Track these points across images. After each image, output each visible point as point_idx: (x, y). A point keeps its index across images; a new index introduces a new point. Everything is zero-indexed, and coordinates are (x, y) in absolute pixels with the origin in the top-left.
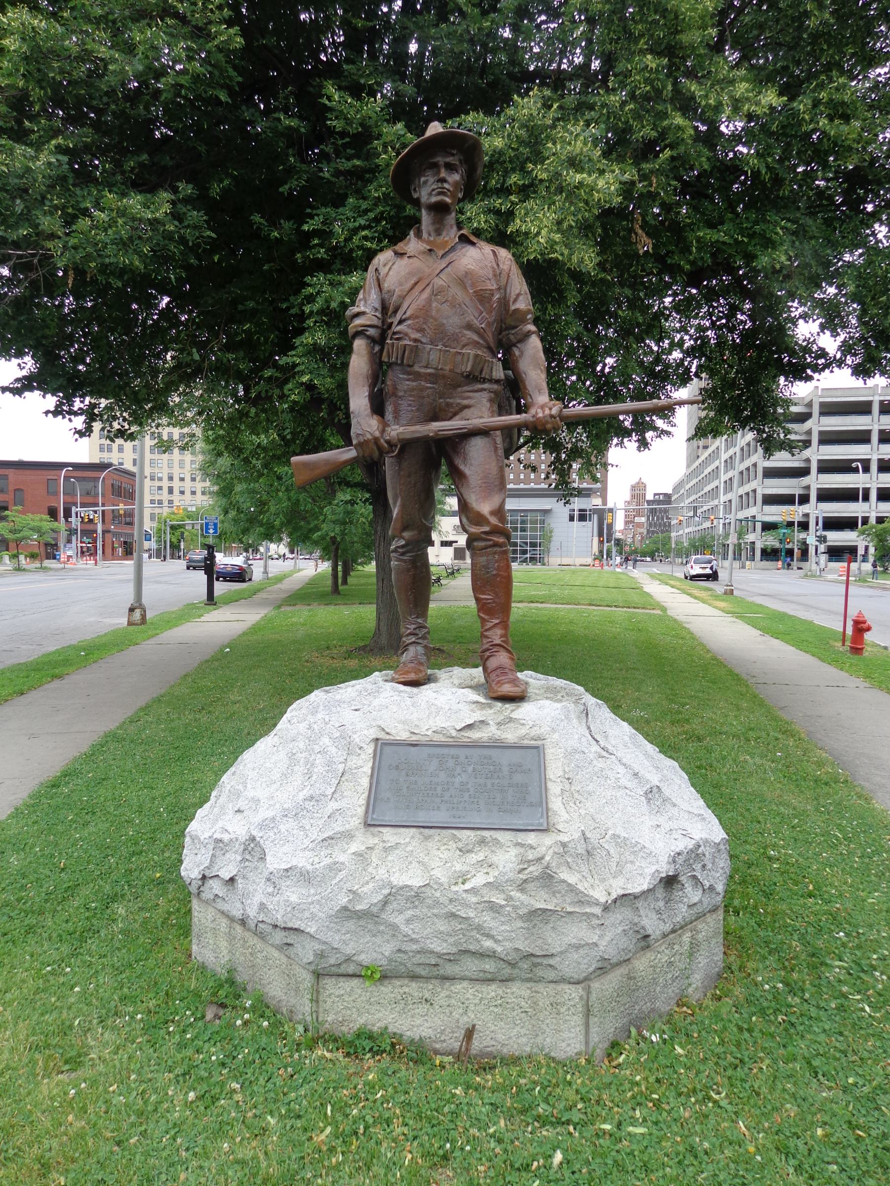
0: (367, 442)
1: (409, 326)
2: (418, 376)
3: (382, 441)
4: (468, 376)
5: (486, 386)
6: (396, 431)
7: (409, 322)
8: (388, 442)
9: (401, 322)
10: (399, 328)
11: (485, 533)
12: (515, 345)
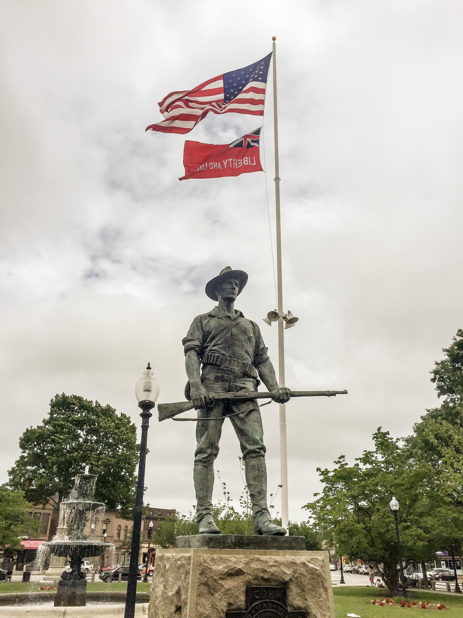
5: (251, 379)
8: (210, 399)
9: (213, 346)
10: (214, 348)
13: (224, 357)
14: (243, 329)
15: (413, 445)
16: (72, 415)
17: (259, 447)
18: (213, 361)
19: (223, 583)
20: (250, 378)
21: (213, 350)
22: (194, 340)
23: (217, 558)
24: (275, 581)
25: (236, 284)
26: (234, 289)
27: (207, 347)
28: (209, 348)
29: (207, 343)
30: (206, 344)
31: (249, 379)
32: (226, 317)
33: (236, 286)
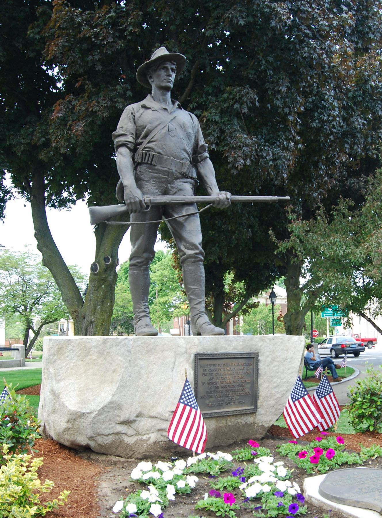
0: (135, 203)
1: (155, 145)
2: (159, 171)
3: (143, 202)
4: (183, 174)
5: (190, 180)
6: (147, 198)
7: (155, 143)
8: (146, 203)
9: (149, 142)
11: (196, 254)
12: (200, 162)
13: (161, 156)
14: (181, 124)
15: (314, 166)
16: (103, 362)
17: (197, 251)
18: (148, 160)
19: (293, 365)
20: (187, 178)
21: (147, 148)
22: (125, 135)
23: (121, 380)
24: (254, 91)
25: (172, 69)
26: (171, 76)
27: (141, 144)
28: (144, 145)
29: (142, 139)
30: (139, 140)
31: (186, 180)
32: (161, 109)
33: (172, 71)
